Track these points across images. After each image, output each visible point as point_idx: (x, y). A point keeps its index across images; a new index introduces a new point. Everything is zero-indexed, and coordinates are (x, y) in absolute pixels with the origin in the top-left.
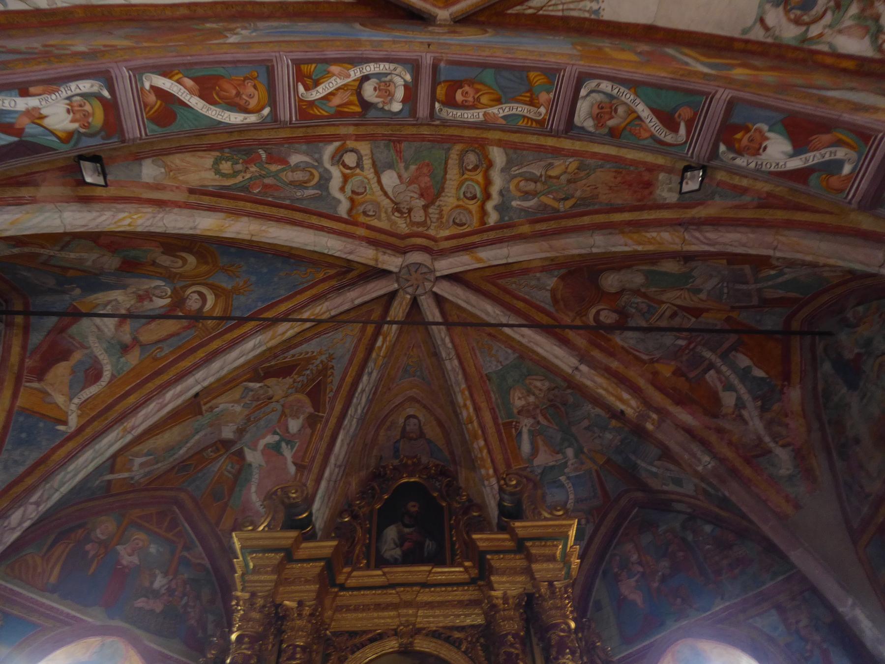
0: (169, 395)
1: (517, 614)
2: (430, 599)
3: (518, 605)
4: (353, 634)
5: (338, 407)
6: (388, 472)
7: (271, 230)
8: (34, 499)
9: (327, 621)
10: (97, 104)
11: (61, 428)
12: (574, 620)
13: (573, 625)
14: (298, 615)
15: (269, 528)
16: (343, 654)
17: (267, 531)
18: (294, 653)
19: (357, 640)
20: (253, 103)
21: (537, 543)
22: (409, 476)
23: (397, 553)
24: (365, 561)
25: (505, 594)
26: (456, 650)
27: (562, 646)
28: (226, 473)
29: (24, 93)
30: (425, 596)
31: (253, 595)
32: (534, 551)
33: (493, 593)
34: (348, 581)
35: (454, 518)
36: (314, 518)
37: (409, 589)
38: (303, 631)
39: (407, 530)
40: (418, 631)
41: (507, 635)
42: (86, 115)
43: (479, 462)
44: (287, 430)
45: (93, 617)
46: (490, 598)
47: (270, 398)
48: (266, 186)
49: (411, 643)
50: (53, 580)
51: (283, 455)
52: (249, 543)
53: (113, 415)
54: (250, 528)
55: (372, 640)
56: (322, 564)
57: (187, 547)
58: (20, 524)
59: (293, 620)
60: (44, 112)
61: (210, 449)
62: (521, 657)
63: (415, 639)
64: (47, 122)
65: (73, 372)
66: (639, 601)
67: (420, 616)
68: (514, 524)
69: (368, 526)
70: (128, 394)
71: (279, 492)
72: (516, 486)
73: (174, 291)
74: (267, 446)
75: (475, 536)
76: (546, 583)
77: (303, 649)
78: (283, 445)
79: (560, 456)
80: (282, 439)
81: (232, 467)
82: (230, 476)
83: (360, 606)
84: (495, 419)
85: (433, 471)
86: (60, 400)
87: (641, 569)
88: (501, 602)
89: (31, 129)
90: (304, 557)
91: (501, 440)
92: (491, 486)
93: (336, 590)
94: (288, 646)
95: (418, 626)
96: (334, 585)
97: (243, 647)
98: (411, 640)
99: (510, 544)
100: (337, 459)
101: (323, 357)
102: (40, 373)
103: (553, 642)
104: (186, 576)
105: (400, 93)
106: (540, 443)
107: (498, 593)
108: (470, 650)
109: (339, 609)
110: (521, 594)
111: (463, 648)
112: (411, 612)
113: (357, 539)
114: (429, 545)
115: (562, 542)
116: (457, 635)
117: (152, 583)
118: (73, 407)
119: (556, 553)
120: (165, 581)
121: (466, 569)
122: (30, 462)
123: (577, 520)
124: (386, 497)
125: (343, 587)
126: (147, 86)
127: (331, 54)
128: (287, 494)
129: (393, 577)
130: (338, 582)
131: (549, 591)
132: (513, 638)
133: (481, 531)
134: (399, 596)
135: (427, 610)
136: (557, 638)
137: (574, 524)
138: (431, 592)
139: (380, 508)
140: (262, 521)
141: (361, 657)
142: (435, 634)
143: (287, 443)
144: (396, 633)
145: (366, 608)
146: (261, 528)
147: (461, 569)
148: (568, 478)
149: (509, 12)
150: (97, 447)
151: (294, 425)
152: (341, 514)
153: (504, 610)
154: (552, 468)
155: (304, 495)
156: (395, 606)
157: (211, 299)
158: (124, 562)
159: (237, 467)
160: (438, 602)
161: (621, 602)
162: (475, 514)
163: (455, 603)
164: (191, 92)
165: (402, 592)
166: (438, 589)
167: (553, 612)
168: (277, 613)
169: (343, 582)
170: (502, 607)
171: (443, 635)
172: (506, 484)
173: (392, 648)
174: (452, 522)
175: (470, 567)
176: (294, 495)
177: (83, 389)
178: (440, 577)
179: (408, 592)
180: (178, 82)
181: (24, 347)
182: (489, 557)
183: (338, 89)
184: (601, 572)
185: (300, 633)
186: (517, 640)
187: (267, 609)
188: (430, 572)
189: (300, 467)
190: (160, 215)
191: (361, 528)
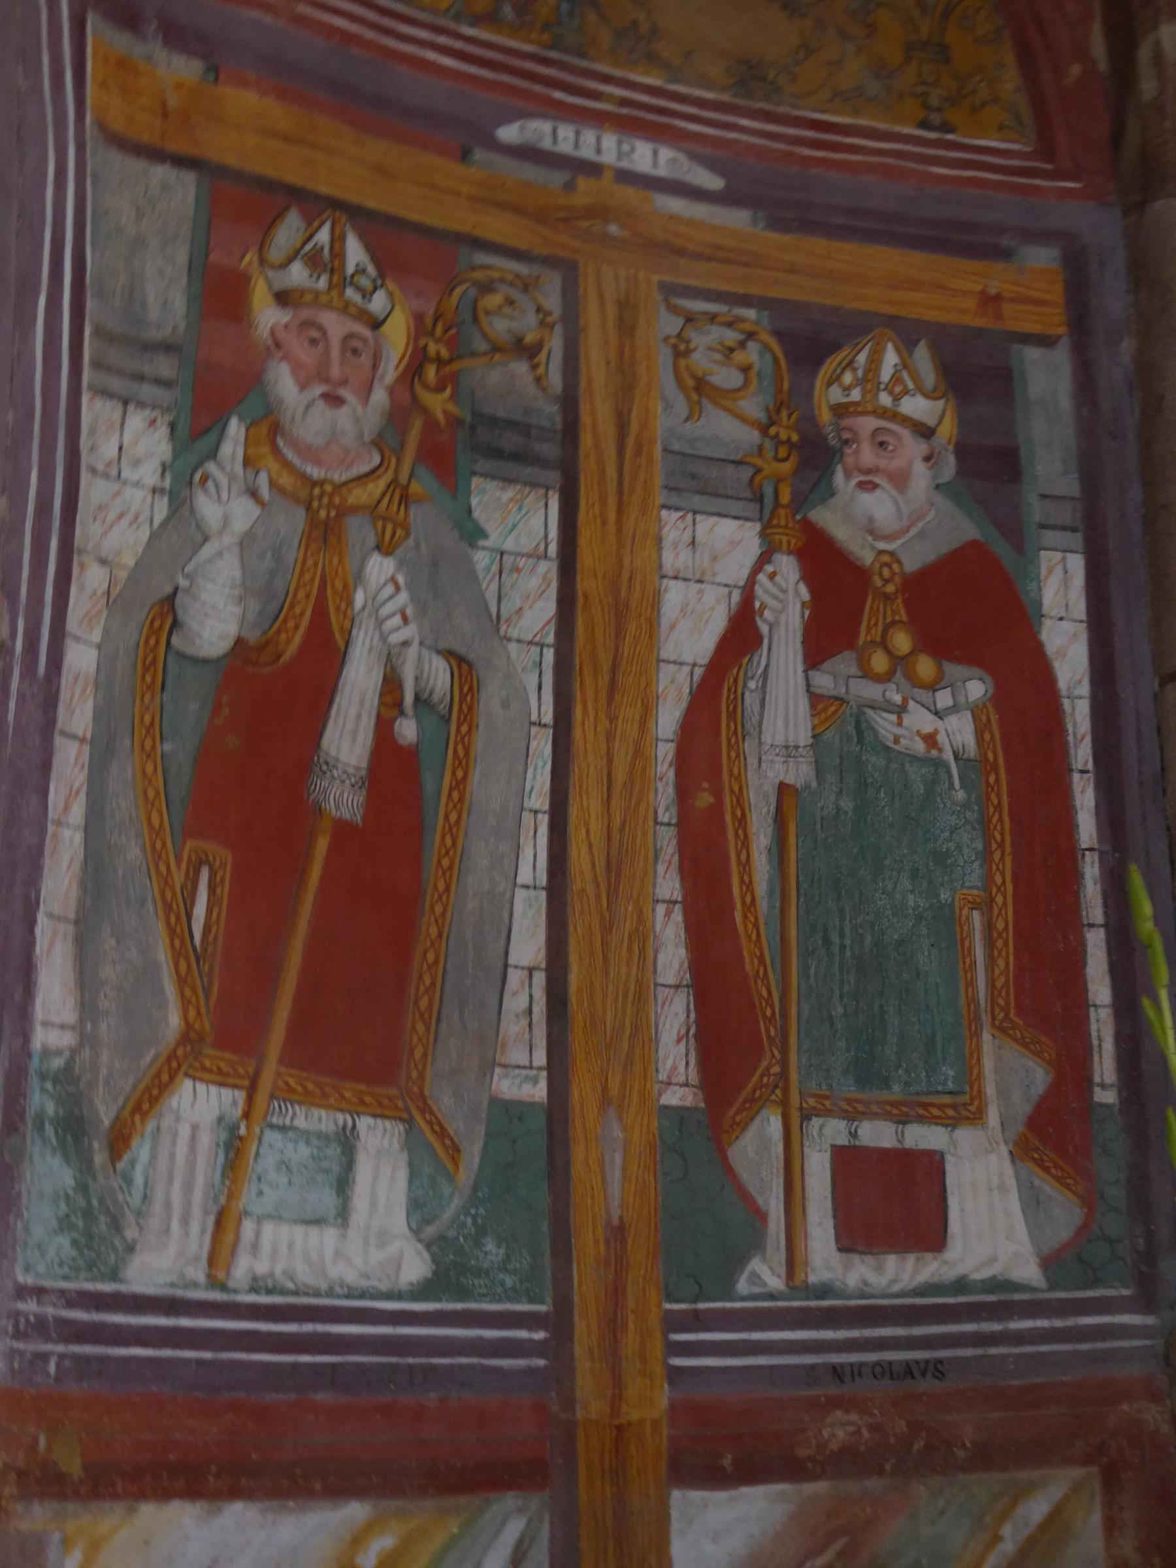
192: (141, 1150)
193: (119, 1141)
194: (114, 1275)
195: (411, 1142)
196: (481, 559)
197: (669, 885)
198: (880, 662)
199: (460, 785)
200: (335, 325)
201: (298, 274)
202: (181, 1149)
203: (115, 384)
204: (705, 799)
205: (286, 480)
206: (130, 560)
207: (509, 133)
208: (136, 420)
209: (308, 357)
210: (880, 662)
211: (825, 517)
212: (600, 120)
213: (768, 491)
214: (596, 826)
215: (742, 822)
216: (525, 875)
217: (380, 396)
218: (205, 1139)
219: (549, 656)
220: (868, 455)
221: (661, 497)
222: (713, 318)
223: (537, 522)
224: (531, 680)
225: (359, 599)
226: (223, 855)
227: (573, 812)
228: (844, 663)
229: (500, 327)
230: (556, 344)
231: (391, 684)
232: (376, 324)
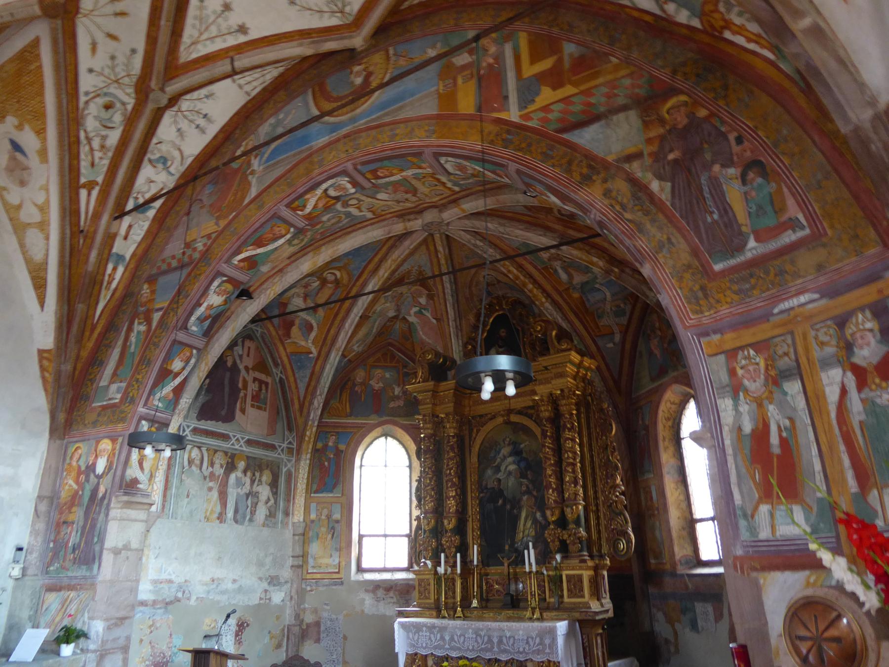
0: (347, 325)
4: (481, 416)
5: (440, 287)
7: (339, 247)
8: (318, 393)
10: (225, 284)
11: (311, 355)
20: (283, 232)
29: (200, 305)
42: (225, 291)
44: (421, 304)
45: (373, 420)
47: (402, 293)
48: (321, 233)
50: (348, 410)
53: (329, 342)
57: (405, 366)
58: (319, 406)
60: (211, 304)
64: (214, 305)
65: (300, 329)
66: (658, 356)
70: (329, 331)
73: (317, 278)
74: (415, 313)
80: (421, 308)
84: (535, 267)
86: (303, 343)
89: (212, 312)
91: (545, 277)
101: (416, 268)
102: (288, 335)
105: (349, 186)
106: (572, 272)
117: (393, 393)
118: (310, 345)
120: (399, 389)
122: (308, 376)
126: (236, 263)
127: (301, 190)
149: (403, 8)
150: (330, 362)
151: (423, 301)
154: (587, 282)
157: (338, 274)
158: (376, 388)
161: (651, 353)
164: (254, 249)
177: (309, 335)
180: (246, 251)
181: (274, 326)
183: (317, 201)
190: (284, 279)
192: (756, 517)
193: (753, 516)
194: (757, 537)
195: (803, 509)
196: (789, 398)
197: (842, 448)
198: (874, 387)
199: (797, 442)
200: (751, 368)
201: (743, 362)
202: (763, 516)
203: (721, 396)
204: (844, 429)
205: (751, 399)
206: (731, 423)
207: (776, 311)
208: (726, 400)
209: (748, 376)
210: (874, 387)
211: (856, 360)
212: (792, 297)
213: (841, 360)
214: (825, 440)
215: (854, 432)
216: (813, 454)
217: (762, 377)
218: (767, 514)
219: (807, 411)
220: (860, 341)
221: (819, 370)
222: (821, 327)
223: (797, 386)
224: (805, 417)
225: (769, 414)
226: (759, 466)
227: (820, 440)
228: (866, 390)
229: (780, 352)
230: (792, 350)
231: (779, 427)
232: (757, 364)
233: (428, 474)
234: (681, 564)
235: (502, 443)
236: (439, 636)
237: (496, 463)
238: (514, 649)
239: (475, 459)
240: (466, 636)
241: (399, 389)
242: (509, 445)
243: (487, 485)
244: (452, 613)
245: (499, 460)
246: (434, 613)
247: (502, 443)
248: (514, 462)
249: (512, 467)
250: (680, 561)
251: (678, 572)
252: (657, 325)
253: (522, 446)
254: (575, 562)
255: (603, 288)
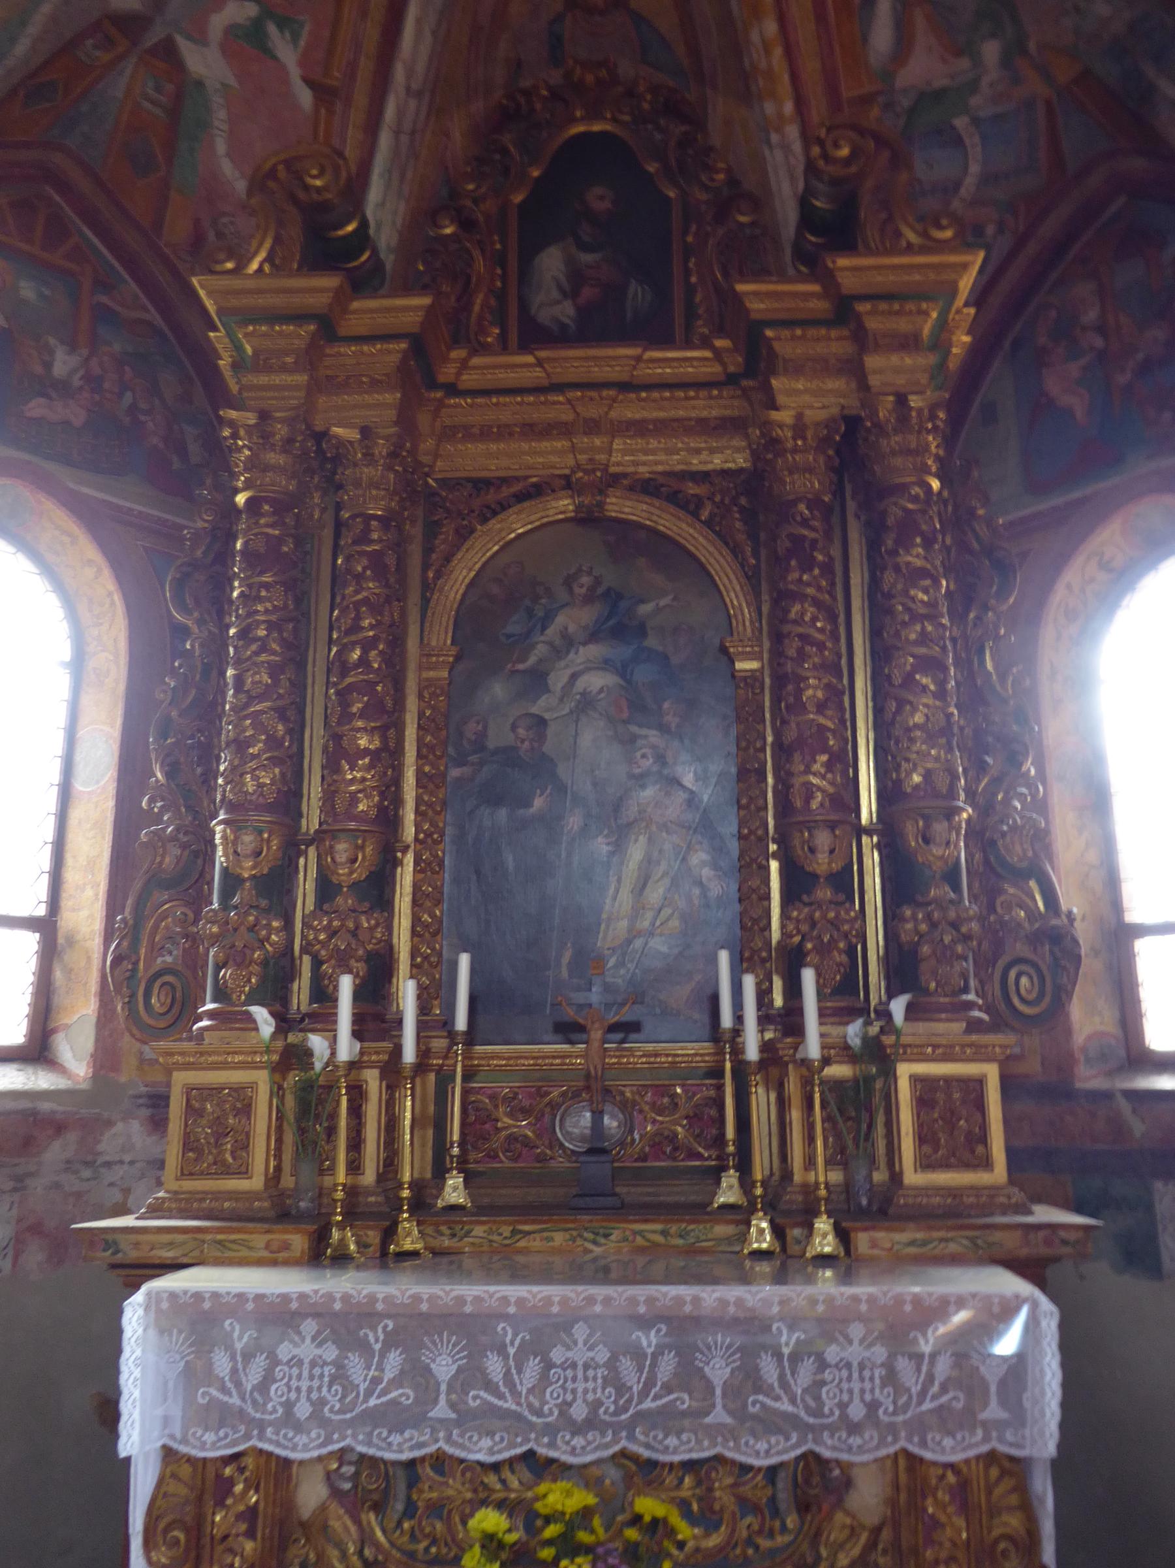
1: (821, 460)
2: (638, 416)
3: (824, 442)
4: (481, 484)
6: (538, 106)
9: (426, 459)
12: (937, 476)
13: (935, 484)
14: (364, 455)
15: (273, 265)
16: (465, 522)
17: (271, 275)
18: (367, 530)
19: (491, 497)
21: (883, 306)
22: (594, 114)
23: (566, 311)
24: (497, 331)
25: (799, 416)
26: (690, 519)
27: (907, 529)
28: (147, 105)
30: (630, 410)
31: (264, 416)
32: (873, 324)
33: (775, 415)
34: (464, 377)
35: (694, 228)
36: (371, 232)
37: (593, 394)
38: (378, 488)
39: (587, 258)
40: (614, 480)
41: (799, 500)
43: (761, 82)
46: (767, 425)
49: (601, 505)
51: (275, 59)
52: (234, 302)
54: (230, 265)
55: (522, 497)
56: (403, 346)
59: (355, 465)
61: (89, 42)
62: (820, 545)
63: (607, 496)
66: (1079, 413)
67: (618, 450)
68: (834, 262)
69: (498, 246)
71: (282, 172)
72: (847, 162)
74: (231, 31)
75: (741, 288)
76: (891, 398)
77: (384, 521)
78: (272, 29)
79: (964, 63)
81: (158, 89)
82: (157, 111)
83: (491, 427)
85: (646, 106)
87: (1099, 342)
88: (790, 434)
90: (363, 331)
92: (786, 148)
93: (439, 394)
94: (353, 517)
95: (612, 470)
96: (433, 385)
97: (262, 521)
98: (598, 498)
99: (820, 306)
100: (410, 73)
103: (890, 521)
104: (117, 347)
107: (784, 416)
108: (717, 519)
109: (449, 433)
110: (833, 419)
111: (705, 515)
112: (598, 442)
113: (474, 279)
114: (637, 294)
115: (941, 303)
116: (692, 489)
117: (48, 366)
119: (921, 329)
120: (74, 361)
121: (718, 354)
123: (981, 255)
124: (536, 174)
125: (452, 389)
128: (301, 179)
129: (559, 370)
130: (441, 379)
131: (894, 415)
132: (807, 508)
133: (761, 273)
134: (573, 407)
135: (630, 437)
136: (900, 513)
137: (974, 263)
138: (644, 400)
139: (524, 202)
140: (252, 250)
141: (501, 530)
142: (648, 487)
143: (282, 24)
144: (568, 484)
145: (503, 432)
146: (254, 266)
147: (708, 354)
148: (976, 121)
152: (433, 216)
153: (795, 450)
154: (939, 95)
155: (342, 182)
156: (564, 430)
159: (170, 87)
160: (656, 421)
162: (743, 219)
163: (693, 423)
165: (578, 399)
166: (655, 395)
167: (898, 461)
168: (320, 451)
169: (451, 379)
170: (790, 445)
171: (663, 489)
172: (825, 156)
173: (561, 513)
174: (690, 239)
175: (727, 350)
176: (318, 183)
178: (659, 371)
179: (591, 399)
182: (769, 333)
184: (1007, 344)
185: (374, 492)
186: (816, 513)
187: (298, 444)
188: (638, 359)
189: (323, 93)
191: (483, 251)
233: (263, 649)
234: (1088, 1060)
235: (562, 595)
236: (394, 1360)
237: (532, 660)
238: (817, 1413)
239: (441, 636)
240: (557, 1355)
241: (74, 361)
242: (589, 599)
243: (483, 735)
244: (373, 1237)
245: (541, 650)
246: (299, 1242)
247: (562, 595)
248: (606, 664)
249: (596, 681)
250: (1084, 1049)
251: (1079, 1085)
252: (1091, 315)
253: (645, 609)
254: (951, 1029)
255: (973, 142)
